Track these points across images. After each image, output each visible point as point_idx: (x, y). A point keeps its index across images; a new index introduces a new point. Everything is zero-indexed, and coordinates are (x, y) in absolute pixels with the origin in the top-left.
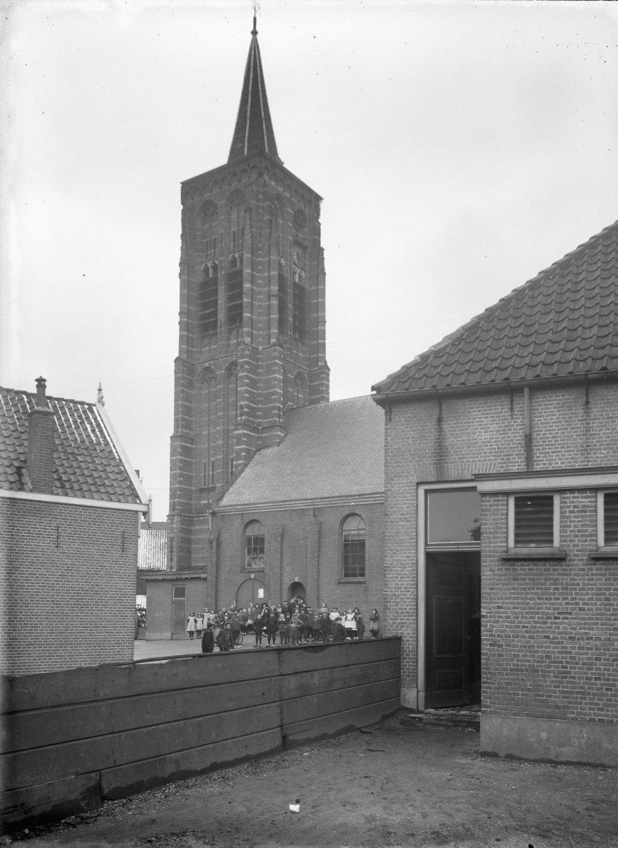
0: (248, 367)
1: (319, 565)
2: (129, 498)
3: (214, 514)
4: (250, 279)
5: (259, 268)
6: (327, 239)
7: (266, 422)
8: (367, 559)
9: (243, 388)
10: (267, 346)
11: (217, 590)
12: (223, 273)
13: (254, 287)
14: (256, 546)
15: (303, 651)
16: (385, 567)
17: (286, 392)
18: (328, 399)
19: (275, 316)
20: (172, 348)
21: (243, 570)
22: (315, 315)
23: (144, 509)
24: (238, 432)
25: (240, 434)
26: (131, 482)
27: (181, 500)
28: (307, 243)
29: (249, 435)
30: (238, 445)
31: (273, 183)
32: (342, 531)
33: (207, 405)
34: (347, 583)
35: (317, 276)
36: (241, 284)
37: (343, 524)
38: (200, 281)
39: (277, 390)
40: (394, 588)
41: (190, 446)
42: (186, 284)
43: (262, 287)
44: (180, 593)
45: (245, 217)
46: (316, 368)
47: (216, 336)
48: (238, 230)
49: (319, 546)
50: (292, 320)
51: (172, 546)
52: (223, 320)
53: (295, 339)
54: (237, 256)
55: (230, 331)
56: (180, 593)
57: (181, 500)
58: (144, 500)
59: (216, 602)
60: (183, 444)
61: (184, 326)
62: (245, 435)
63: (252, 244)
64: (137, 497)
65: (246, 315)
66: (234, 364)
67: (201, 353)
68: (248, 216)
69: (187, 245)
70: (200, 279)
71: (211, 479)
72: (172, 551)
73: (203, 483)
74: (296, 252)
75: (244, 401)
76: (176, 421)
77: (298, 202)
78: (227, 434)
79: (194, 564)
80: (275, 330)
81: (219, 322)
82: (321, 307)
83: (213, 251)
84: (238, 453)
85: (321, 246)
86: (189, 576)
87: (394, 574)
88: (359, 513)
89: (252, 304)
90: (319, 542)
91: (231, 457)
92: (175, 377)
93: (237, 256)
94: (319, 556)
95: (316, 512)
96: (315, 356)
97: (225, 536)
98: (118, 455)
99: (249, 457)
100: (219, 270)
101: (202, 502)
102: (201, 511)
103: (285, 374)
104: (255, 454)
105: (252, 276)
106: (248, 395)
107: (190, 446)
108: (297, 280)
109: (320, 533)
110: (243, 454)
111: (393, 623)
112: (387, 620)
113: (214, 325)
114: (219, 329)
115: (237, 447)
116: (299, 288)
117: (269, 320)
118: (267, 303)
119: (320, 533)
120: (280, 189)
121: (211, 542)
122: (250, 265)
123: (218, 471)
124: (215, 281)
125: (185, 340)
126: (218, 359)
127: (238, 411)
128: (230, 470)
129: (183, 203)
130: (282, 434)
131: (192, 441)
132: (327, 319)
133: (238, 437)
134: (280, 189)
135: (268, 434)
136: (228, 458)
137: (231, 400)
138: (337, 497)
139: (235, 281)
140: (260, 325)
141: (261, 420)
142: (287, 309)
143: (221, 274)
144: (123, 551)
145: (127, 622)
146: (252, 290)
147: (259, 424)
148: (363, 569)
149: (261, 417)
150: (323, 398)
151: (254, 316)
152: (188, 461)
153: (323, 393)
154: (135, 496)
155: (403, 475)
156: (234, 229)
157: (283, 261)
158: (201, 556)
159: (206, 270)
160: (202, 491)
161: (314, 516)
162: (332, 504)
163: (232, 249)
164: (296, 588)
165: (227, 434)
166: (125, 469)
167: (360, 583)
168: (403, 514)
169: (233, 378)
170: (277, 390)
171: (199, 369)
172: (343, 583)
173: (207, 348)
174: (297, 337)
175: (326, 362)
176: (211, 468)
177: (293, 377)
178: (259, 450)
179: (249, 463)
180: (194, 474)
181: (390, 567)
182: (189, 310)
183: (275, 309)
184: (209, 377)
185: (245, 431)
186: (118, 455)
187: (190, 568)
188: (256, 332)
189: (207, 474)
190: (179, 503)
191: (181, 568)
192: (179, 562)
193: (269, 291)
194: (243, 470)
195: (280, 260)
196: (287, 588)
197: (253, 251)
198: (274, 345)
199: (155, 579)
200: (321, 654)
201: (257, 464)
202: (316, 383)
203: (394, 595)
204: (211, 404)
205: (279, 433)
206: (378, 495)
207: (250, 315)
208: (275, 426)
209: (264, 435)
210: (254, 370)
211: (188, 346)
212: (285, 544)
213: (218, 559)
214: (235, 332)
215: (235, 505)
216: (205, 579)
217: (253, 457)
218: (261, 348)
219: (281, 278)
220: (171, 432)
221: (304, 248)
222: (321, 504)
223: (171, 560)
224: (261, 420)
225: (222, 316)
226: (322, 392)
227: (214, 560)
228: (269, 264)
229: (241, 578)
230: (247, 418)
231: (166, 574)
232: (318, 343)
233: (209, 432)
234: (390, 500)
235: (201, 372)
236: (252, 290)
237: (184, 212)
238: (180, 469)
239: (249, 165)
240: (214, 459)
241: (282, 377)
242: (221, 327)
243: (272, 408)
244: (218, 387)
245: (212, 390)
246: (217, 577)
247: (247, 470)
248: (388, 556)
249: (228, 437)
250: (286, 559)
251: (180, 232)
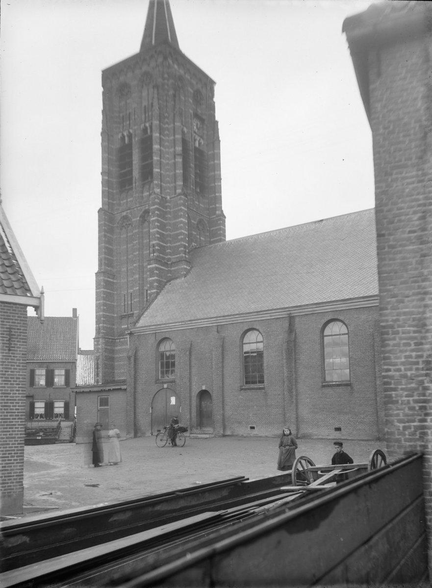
0: (158, 212)
1: (223, 375)
2: (18, 291)
3: (131, 334)
4: (159, 141)
5: (165, 133)
6: (220, 115)
7: (174, 258)
8: (265, 368)
9: (155, 230)
10: (173, 196)
11: (135, 399)
12: (136, 139)
13: (162, 148)
14: (167, 364)
15: (283, 534)
16: (384, 327)
17: (190, 235)
18: (225, 240)
19: (179, 171)
20: (96, 201)
21: (157, 381)
22: (213, 173)
23: (35, 302)
24: (151, 266)
25: (152, 268)
26: (23, 275)
27: (105, 325)
28: (204, 117)
29: (161, 269)
30: (151, 277)
31: (176, 66)
32: (243, 344)
33: (125, 247)
34: (249, 389)
35: (213, 143)
36: (151, 145)
37: (244, 337)
38: (118, 146)
39: (183, 231)
40: (403, 364)
41: (112, 280)
42: (106, 149)
43: (169, 183)
44: (104, 402)
45: (154, 93)
46: (215, 216)
47: (132, 190)
48: (148, 104)
49: (223, 358)
50: (193, 177)
51: (98, 363)
52: (137, 177)
53: (197, 193)
54: (147, 125)
55: (143, 185)
56: (104, 402)
57: (105, 325)
58: (36, 293)
59: (135, 410)
60: (106, 279)
61: (106, 184)
62: (157, 268)
63: (160, 113)
64: (29, 290)
65: (156, 170)
66: (147, 212)
67: (119, 205)
68: (156, 91)
69: (107, 119)
70: (117, 145)
71: (130, 307)
72: (98, 368)
73: (123, 311)
74: (195, 123)
75: (155, 240)
76: (100, 260)
77: (197, 83)
78: (142, 270)
79: (117, 378)
80: (180, 183)
81: (134, 179)
82: (217, 167)
83: (128, 123)
84: (151, 283)
85: (216, 120)
86: (112, 388)
87: (401, 339)
88: (257, 328)
89: (161, 162)
90: (223, 353)
91: (146, 288)
92: (99, 224)
93: (147, 125)
94: (223, 367)
95: (219, 329)
96: (213, 206)
97: (141, 353)
98: (12, 250)
99: (161, 287)
100: (133, 136)
101: (123, 327)
102: (122, 334)
103: (189, 218)
104: (166, 285)
105: (160, 139)
106: (159, 236)
107: (112, 280)
108: (197, 145)
109: (223, 346)
110: (156, 284)
111: (405, 428)
112: (392, 423)
113: (130, 182)
114: (134, 185)
115: (151, 279)
116: (199, 152)
117: (175, 175)
118: (173, 161)
119: (223, 346)
120: (182, 72)
121: (129, 358)
122: (159, 118)
123: (135, 300)
124: (130, 146)
125: (108, 194)
126: (134, 209)
127: (151, 249)
128: (145, 299)
129: (103, 86)
130: (189, 268)
131: (114, 277)
132: (222, 177)
133: (151, 270)
134: (182, 72)
135: (176, 268)
136: (143, 289)
137: (145, 241)
138: (237, 314)
139: (146, 144)
140: (168, 179)
141: (170, 256)
142: (190, 167)
143: (136, 140)
144: (9, 350)
145: (15, 431)
146: (160, 150)
147: (169, 260)
148: (262, 377)
149: (170, 254)
150: (221, 240)
151: (162, 172)
152: (110, 293)
153: (221, 236)
154: (25, 289)
155: (410, 163)
156: (145, 103)
157: (185, 130)
158: (122, 372)
159: (123, 138)
160: (122, 317)
161: (218, 332)
162: (233, 321)
163: (143, 119)
164: (204, 395)
165: (142, 270)
166: (18, 264)
167: (260, 389)
168: (414, 232)
169: (146, 223)
170: (183, 231)
171: (118, 217)
172: (245, 389)
173: (125, 201)
174: (199, 191)
175: (222, 211)
176: (129, 298)
177: (196, 223)
178: (169, 281)
179: (160, 292)
180: (115, 304)
181: (392, 327)
182: (109, 170)
183: (180, 165)
184: (126, 224)
185: (157, 265)
186: (12, 250)
187: (114, 382)
188: (164, 185)
189: (126, 303)
190: (104, 327)
191: (106, 382)
192: (104, 376)
193: (175, 152)
194: (156, 297)
195: (183, 129)
196: (196, 395)
197: (161, 118)
198: (180, 194)
199: (83, 391)
200: (324, 528)
201: (167, 292)
202: (215, 228)
203: (405, 376)
204: (129, 245)
205: (185, 266)
206: (273, 311)
207: (159, 170)
208: (182, 261)
209: (173, 269)
210: (163, 215)
211: (109, 199)
212: (193, 357)
213: (136, 372)
214: (148, 187)
215: (150, 326)
216: (125, 390)
217: (164, 287)
218: (168, 197)
219: (184, 142)
220: (96, 269)
221: (202, 121)
222: (223, 322)
223: (97, 375)
224: (170, 256)
225: (136, 174)
226: (220, 235)
227: (133, 372)
228: (174, 130)
229: (155, 388)
230: (158, 254)
231: (94, 386)
232: (216, 196)
233: (127, 268)
234: (385, 209)
235: (120, 220)
236: (160, 150)
237: (104, 93)
238: (104, 299)
239: (156, 52)
240: (132, 291)
241: (187, 221)
242: (136, 183)
243: (178, 235)
244: (134, 231)
245: (129, 234)
246: (135, 388)
247: (159, 297)
248: (389, 307)
249: (143, 272)
250: (194, 370)
251: (101, 108)
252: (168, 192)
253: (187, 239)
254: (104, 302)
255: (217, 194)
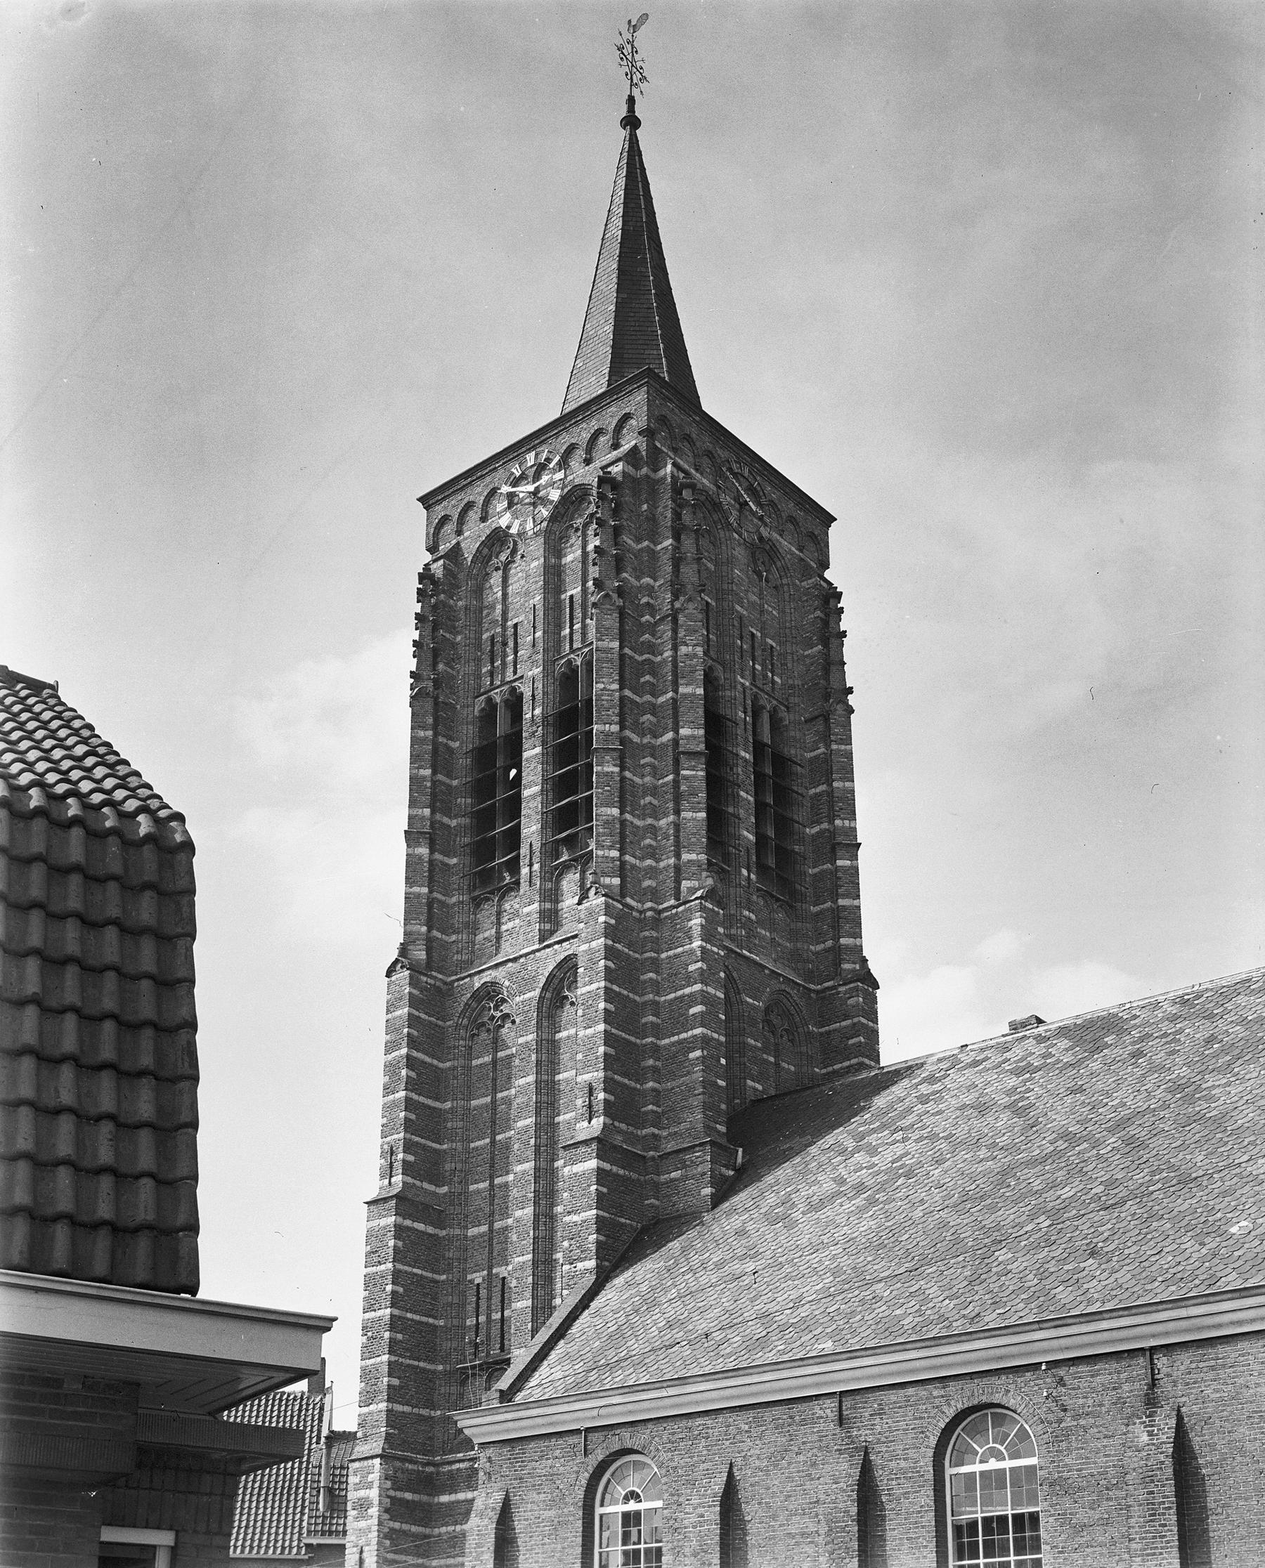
19: (696, 816)
176: (496, 1300)
232: (830, 793)
252: (648, 682)
253: (723, 1061)
254: (396, 1312)
255: (838, 822)
